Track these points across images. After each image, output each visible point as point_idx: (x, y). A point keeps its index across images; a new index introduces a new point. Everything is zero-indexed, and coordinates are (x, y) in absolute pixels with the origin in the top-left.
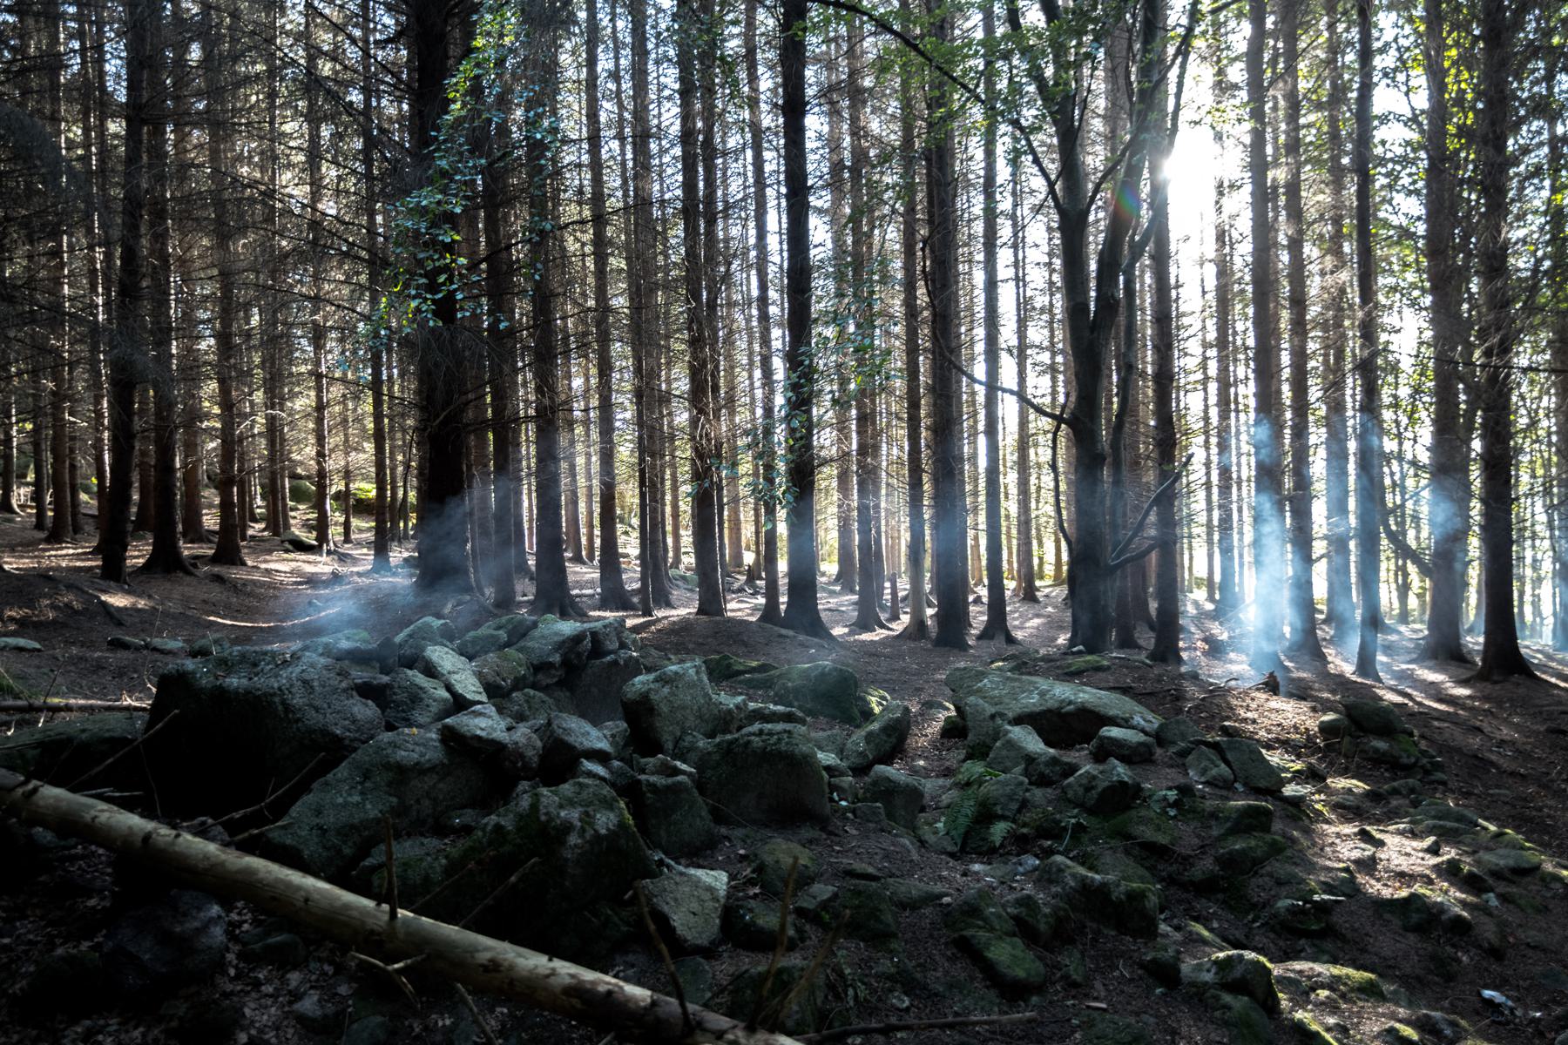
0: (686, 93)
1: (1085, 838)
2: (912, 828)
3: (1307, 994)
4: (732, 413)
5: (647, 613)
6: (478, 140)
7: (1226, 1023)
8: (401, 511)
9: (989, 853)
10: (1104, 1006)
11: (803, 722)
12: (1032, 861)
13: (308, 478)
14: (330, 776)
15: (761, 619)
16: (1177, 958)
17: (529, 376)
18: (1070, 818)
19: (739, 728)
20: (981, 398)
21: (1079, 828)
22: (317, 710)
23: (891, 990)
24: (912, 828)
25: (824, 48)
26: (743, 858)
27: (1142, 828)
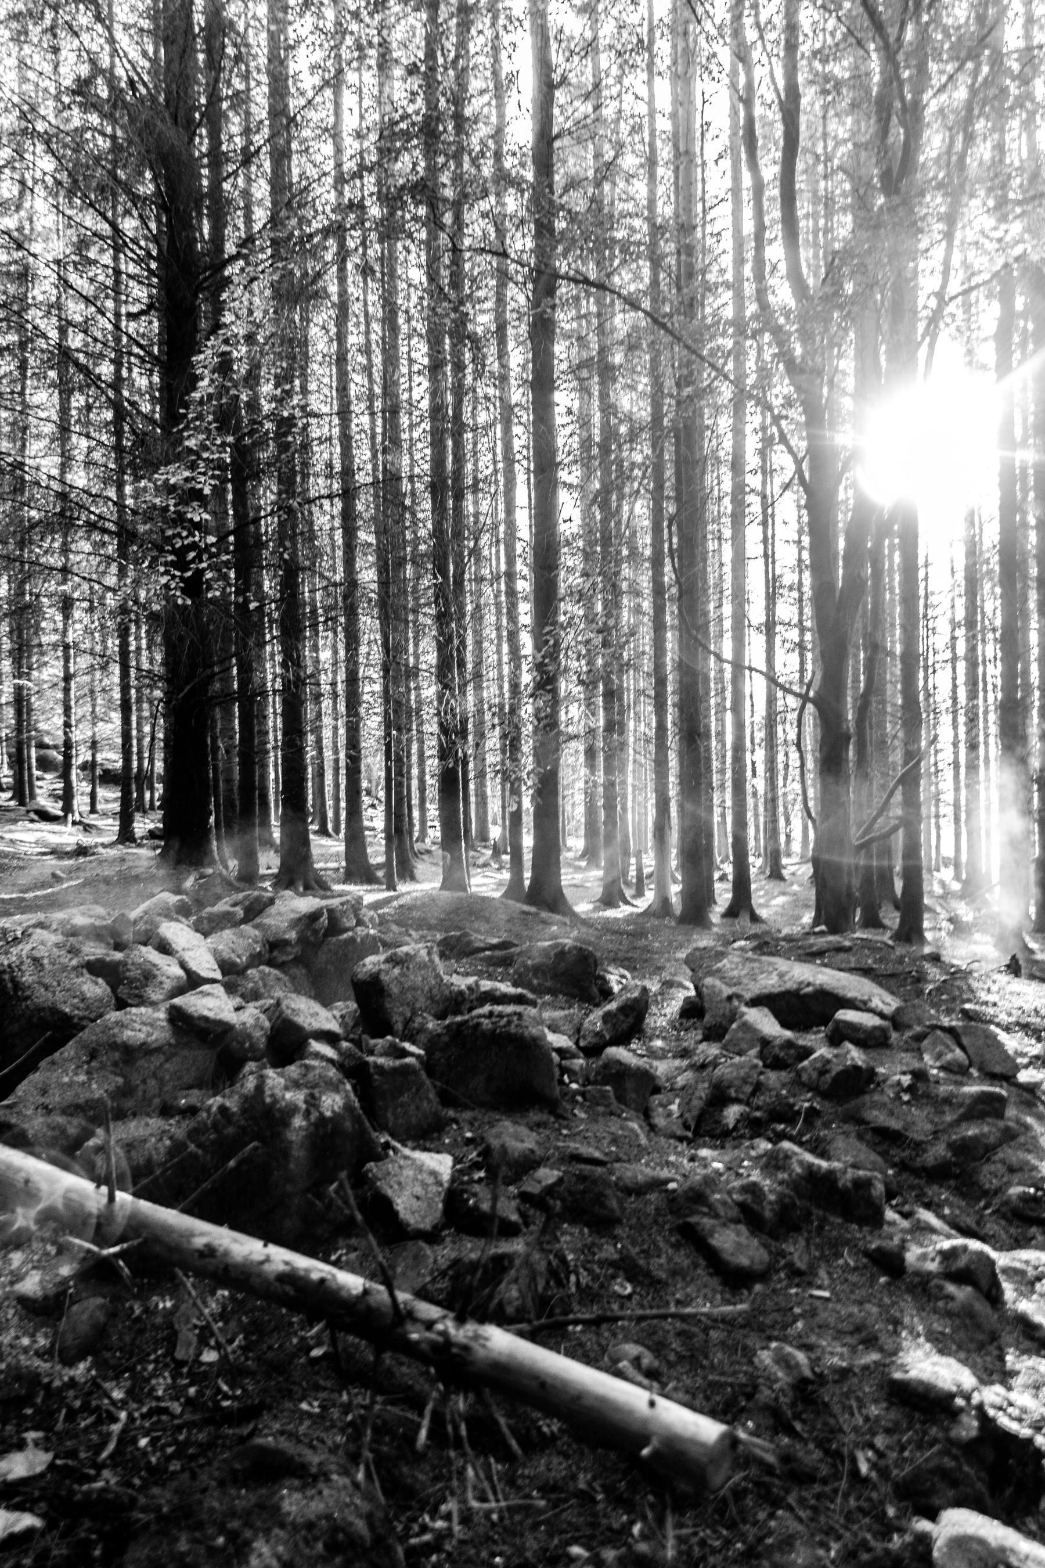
0: (435, 368)
1: (818, 1123)
2: (646, 1114)
3: (1032, 1284)
4: (478, 688)
5: (391, 887)
6: (226, 418)
7: (949, 1314)
8: (144, 779)
9: (721, 1137)
10: (826, 1294)
11: (534, 1004)
12: (764, 1145)
13: (56, 747)
14: (57, 1054)
15: (506, 895)
16: (903, 1247)
17: (278, 648)
18: (804, 1104)
19: (470, 1010)
20: (728, 676)
21: (812, 1113)
22: (47, 987)
23: (614, 1277)
24: (646, 1114)
25: (575, 325)
26: (469, 1142)
27: (875, 1113)
